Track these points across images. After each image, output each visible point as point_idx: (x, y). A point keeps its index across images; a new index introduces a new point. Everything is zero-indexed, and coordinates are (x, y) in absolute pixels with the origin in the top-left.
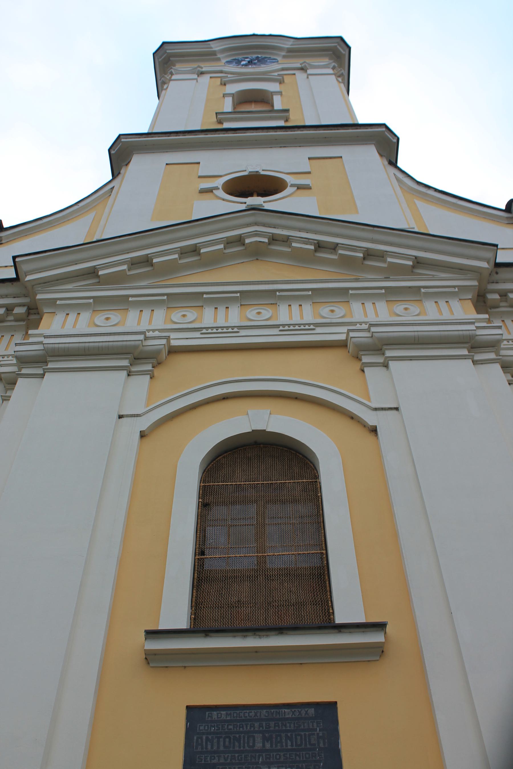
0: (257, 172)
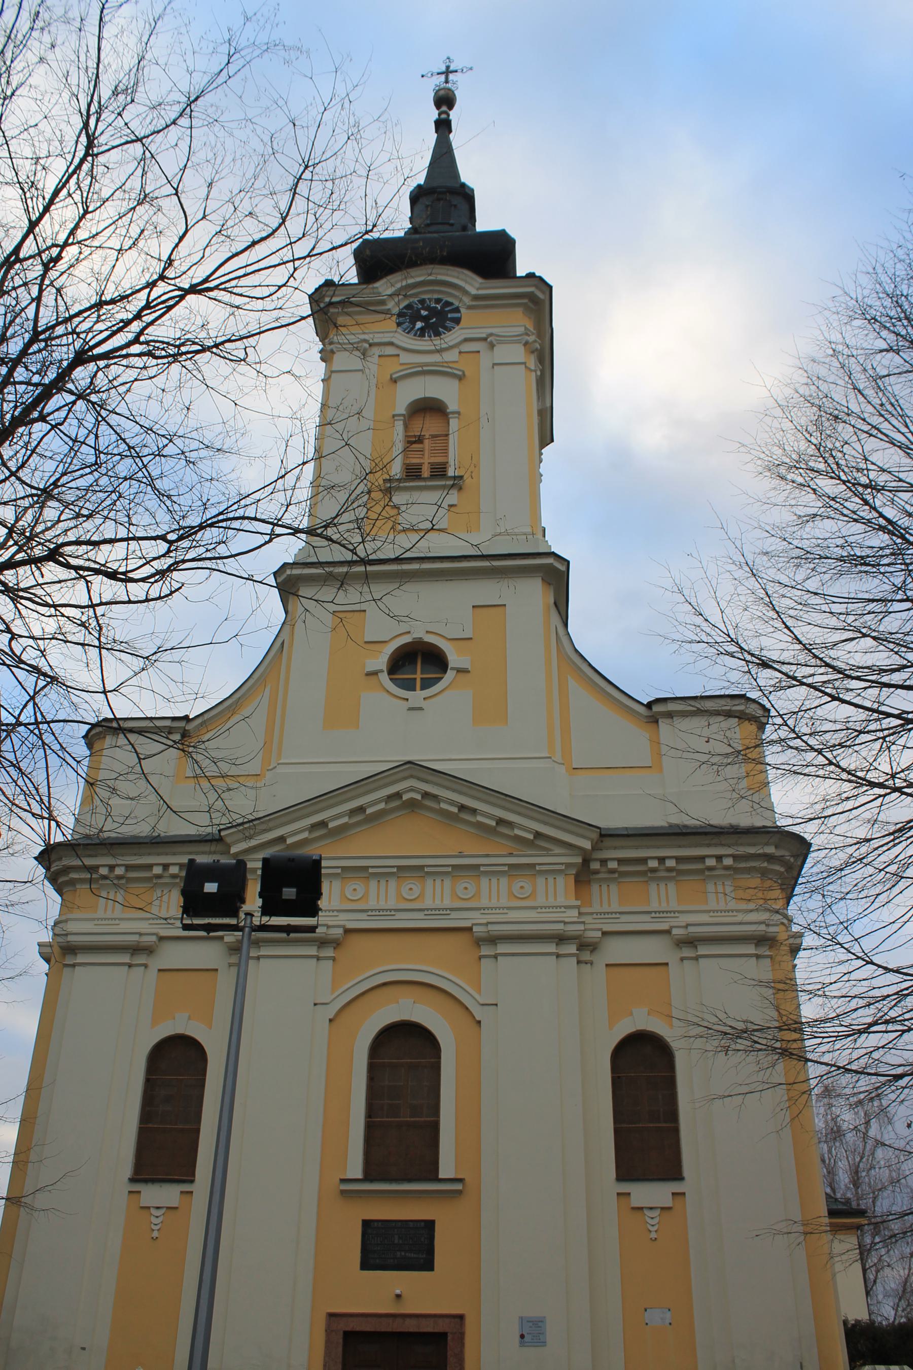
0: (421, 638)
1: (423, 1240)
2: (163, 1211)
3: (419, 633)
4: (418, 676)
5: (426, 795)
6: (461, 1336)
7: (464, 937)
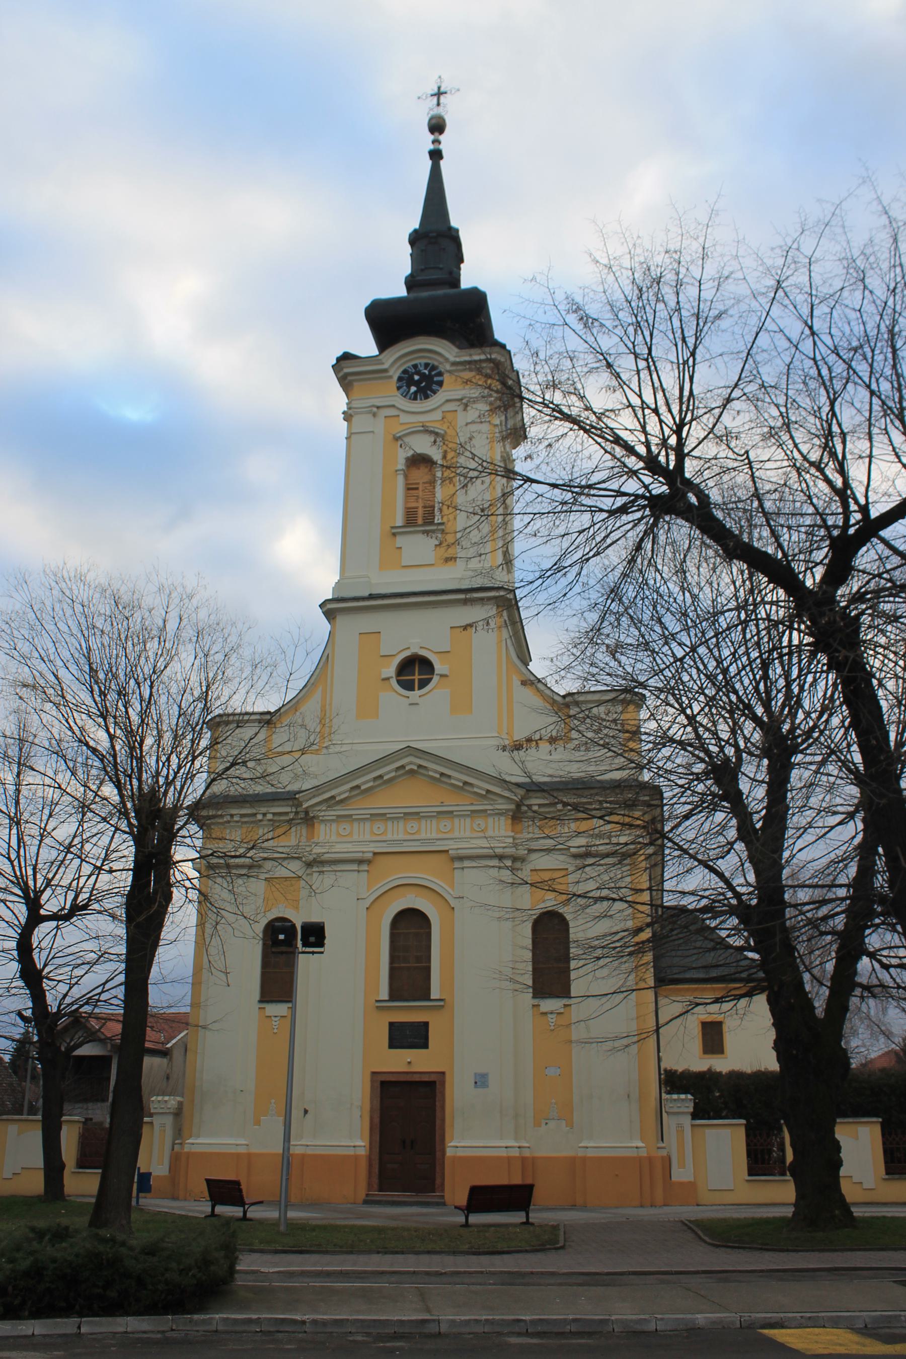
3: (415, 650)
4: (417, 677)
5: (420, 766)
6: (443, 1083)
7: (443, 856)
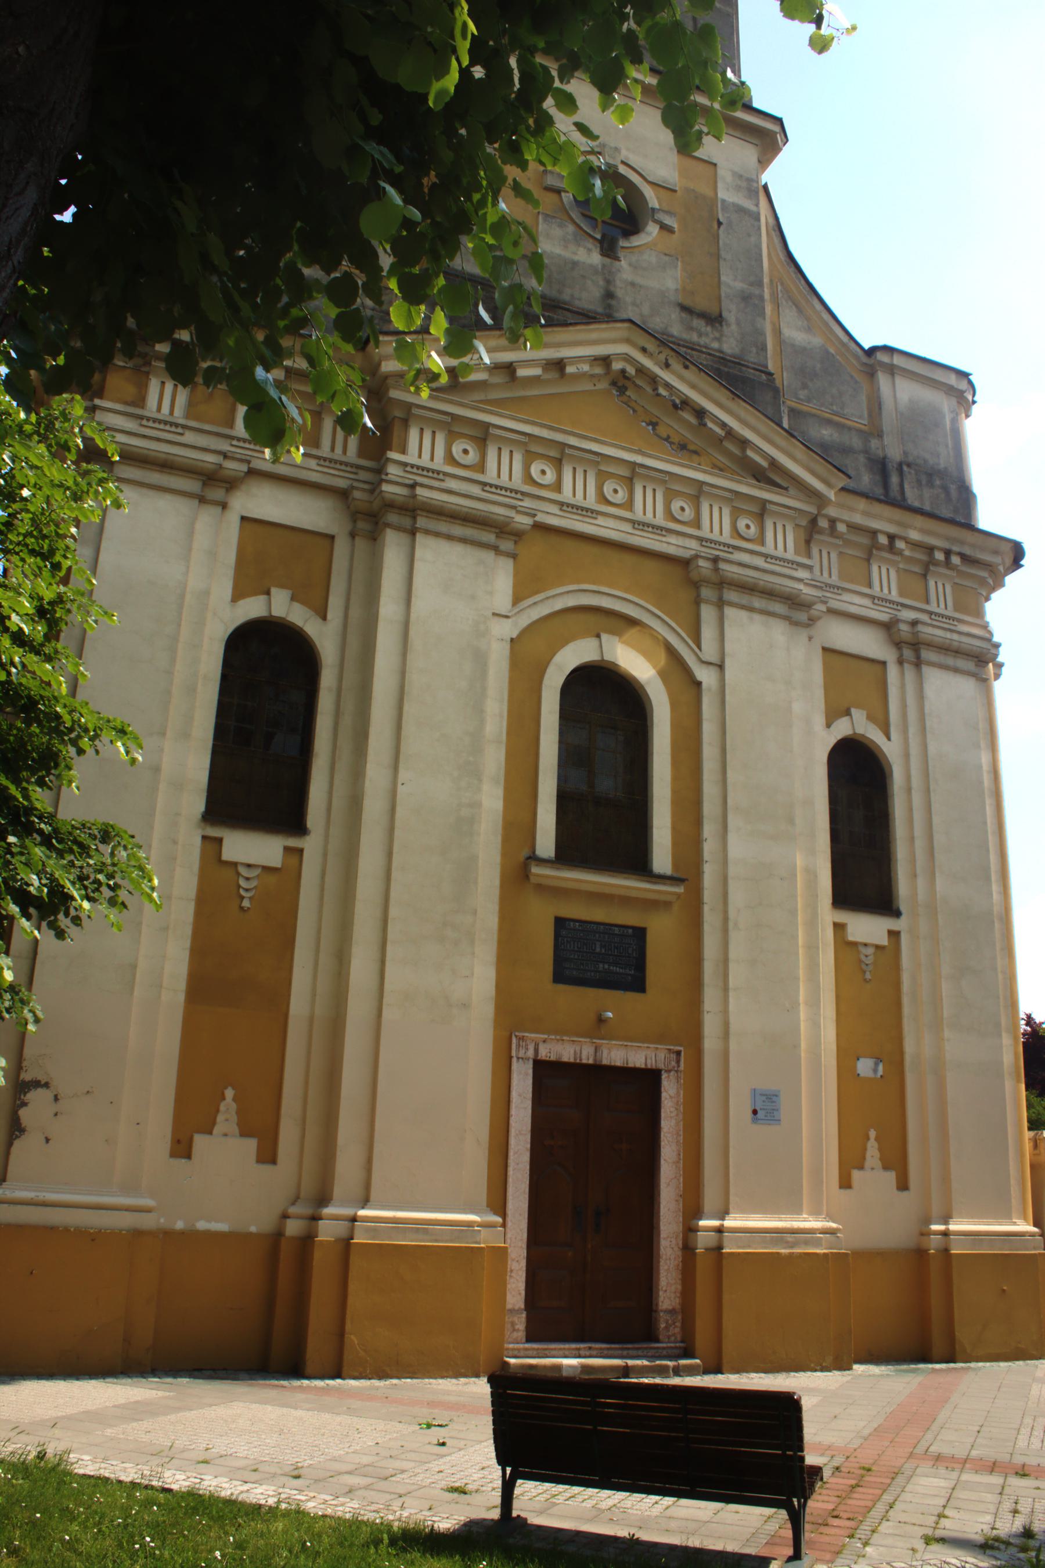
1: (630, 951)
2: (258, 871)
